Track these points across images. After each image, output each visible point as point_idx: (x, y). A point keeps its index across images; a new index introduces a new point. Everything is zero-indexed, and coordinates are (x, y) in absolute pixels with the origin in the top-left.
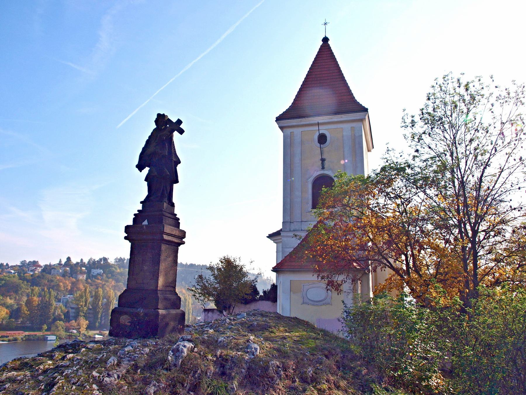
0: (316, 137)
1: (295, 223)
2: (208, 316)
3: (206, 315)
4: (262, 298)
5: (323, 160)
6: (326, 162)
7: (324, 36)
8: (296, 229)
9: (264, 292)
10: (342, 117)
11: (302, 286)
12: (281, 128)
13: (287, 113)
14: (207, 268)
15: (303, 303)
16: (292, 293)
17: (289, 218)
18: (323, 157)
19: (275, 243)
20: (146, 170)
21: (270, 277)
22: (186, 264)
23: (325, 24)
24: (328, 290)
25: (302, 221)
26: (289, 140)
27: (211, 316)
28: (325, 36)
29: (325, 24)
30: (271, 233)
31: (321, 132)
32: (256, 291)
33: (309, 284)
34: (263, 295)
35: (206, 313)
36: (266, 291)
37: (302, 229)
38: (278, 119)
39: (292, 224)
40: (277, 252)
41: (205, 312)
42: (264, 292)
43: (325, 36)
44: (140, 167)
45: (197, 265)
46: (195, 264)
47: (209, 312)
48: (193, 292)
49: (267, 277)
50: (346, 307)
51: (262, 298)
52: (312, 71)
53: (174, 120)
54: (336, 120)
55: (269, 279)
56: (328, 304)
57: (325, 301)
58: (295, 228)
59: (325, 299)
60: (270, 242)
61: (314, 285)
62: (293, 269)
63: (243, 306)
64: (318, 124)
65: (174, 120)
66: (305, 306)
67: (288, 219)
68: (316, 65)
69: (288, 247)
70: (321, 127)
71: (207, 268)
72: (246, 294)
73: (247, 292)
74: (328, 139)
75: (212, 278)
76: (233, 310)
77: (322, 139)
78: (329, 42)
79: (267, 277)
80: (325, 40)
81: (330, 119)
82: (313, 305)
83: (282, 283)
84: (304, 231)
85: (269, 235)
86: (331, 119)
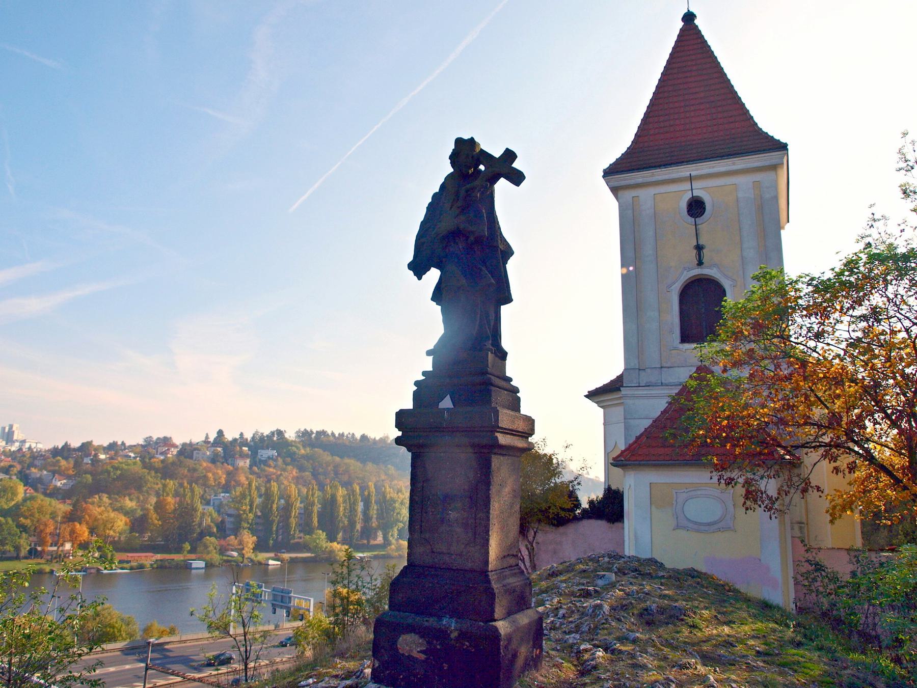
0: (684, 205)
5: (699, 248)
6: (705, 252)
7: (686, 11)
9: (591, 502)
10: (734, 164)
12: (615, 190)
15: (678, 527)
16: (653, 507)
18: (700, 243)
20: (433, 275)
24: (747, 509)
25: (662, 367)
28: (689, 11)
30: (592, 388)
31: (696, 193)
32: (577, 504)
33: (688, 490)
34: (587, 506)
36: (595, 500)
37: (663, 382)
38: (608, 173)
39: (642, 374)
42: (591, 502)
43: (689, 11)
44: (418, 268)
53: (497, 153)
56: (728, 529)
60: (592, 406)
61: (699, 492)
64: (691, 179)
65: (497, 153)
66: (682, 533)
70: (696, 184)
72: (563, 509)
77: (696, 207)
78: (696, 22)
80: (689, 18)
81: (710, 168)
82: (698, 531)
83: (633, 487)
85: (589, 392)
86: (713, 167)
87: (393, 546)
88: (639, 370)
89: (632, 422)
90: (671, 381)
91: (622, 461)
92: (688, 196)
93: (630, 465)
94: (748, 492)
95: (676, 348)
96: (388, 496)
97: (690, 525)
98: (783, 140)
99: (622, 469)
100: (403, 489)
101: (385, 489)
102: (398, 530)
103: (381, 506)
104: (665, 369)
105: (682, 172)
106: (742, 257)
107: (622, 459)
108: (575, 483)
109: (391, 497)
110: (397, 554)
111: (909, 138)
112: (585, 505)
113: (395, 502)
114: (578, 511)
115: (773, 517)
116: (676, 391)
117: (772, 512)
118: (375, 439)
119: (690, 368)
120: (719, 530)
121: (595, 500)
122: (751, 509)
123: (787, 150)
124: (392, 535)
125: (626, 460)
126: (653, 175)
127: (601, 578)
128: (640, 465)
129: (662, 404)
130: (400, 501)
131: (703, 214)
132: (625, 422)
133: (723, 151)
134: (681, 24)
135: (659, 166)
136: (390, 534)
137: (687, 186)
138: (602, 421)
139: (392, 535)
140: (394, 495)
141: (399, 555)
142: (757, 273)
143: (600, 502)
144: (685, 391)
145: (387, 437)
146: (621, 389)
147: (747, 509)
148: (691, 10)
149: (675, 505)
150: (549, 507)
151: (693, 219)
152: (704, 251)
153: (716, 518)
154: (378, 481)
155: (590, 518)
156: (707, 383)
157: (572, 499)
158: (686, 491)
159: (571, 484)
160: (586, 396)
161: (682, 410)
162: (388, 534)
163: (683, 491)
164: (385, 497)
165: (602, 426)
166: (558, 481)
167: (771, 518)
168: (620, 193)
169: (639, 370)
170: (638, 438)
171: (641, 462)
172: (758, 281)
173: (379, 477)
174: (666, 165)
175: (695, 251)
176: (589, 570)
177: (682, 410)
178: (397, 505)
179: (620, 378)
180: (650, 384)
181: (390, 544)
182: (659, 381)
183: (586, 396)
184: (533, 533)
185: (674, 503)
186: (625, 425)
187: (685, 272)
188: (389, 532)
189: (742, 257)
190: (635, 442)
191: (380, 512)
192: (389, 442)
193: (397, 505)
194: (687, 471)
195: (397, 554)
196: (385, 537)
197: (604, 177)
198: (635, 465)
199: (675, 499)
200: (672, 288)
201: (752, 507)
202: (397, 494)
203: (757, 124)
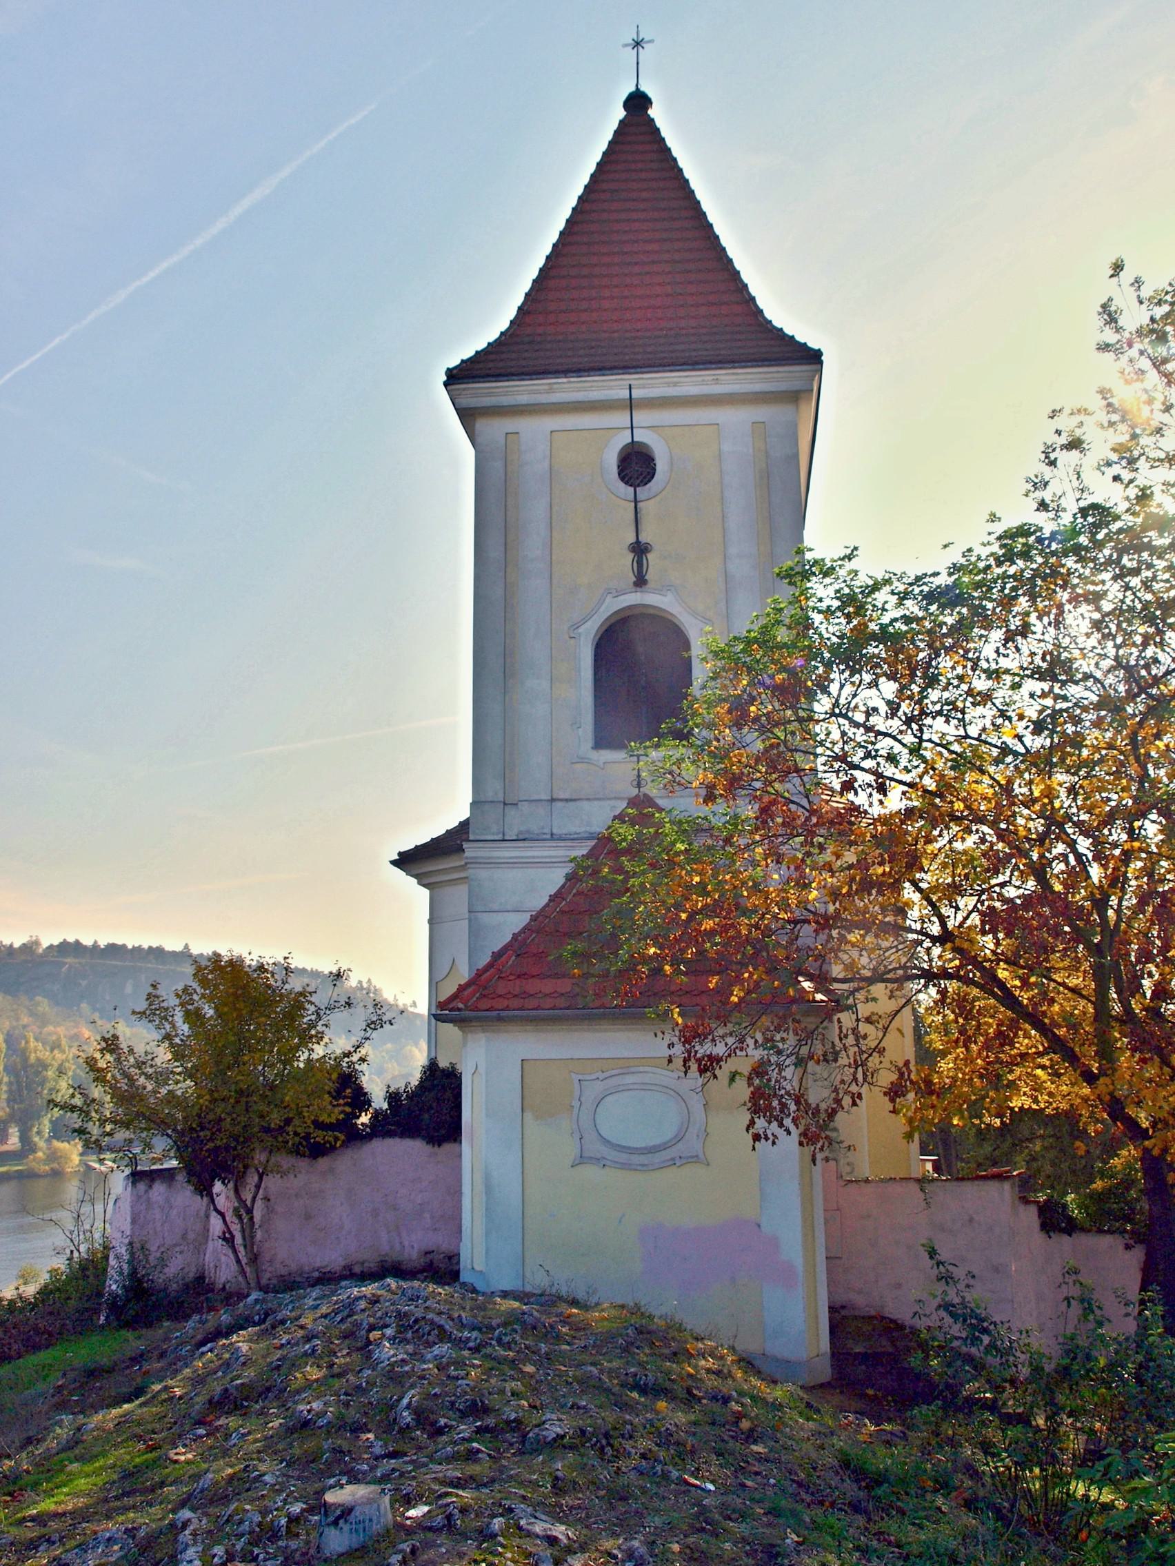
1: (524, 807)
2: (148, 1200)
3: (139, 1197)
4: (385, 1126)
5: (640, 550)
7: (633, 89)
8: (528, 832)
9: (393, 1097)
11: (577, 1086)
12: (467, 416)
13: (492, 357)
14: (134, 1013)
15: (582, 1159)
16: (529, 1116)
17: (498, 785)
18: (643, 538)
19: (424, 886)
21: (369, 981)
22: (95, 946)
23: (638, 44)
24: (757, 1138)
25: (553, 800)
26: (498, 465)
27: (161, 1199)
28: (637, 89)
29: (638, 44)
30: (408, 845)
32: (361, 1100)
33: (606, 1074)
34: (385, 1106)
35: (142, 1186)
36: (401, 1090)
37: (555, 831)
38: (454, 378)
39: (511, 812)
40: (431, 921)
41: (134, 1183)
42: (393, 1097)
43: (637, 89)
45: (130, 947)
46: (124, 946)
47: (153, 1180)
48: (75, 1115)
49: (360, 982)
50: (947, 1278)
51: (385, 1126)
52: (587, 206)
54: (694, 390)
55: (365, 985)
56: (695, 1159)
57: (674, 1149)
58: (522, 828)
59: (679, 1138)
60: (406, 883)
61: (630, 1079)
62: (535, 1013)
63: (303, 1164)
64: (631, 405)
66: (590, 1172)
67: (494, 789)
68: (604, 186)
69: (496, 907)
70: (641, 417)
71: (134, 1013)
72: (318, 1125)
73: (324, 1118)
74: (661, 465)
75: (163, 1055)
76: (258, 1187)
79: (360, 982)
80: (638, 103)
81: (668, 384)
82: (626, 1166)
83: (482, 1069)
84: (561, 839)
85: (400, 854)
86: (675, 384)
87: (40, 1154)
88: (505, 804)
89: (486, 919)
90: (573, 829)
91: (459, 1010)
92: (625, 438)
93: (478, 1019)
94: (756, 1095)
95: (583, 760)
96: (33, 1056)
97: (612, 1155)
98: (813, 345)
99: (460, 1028)
100: (64, 1042)
101: (27, 1042)
102: (51, 1121)
103: (17, 1076)
104: (560, 804)
105: (611, 388)
106: (727, 576)
107: (461, 1005)
108: (355, 1058)
109: (38, 1059)
110: (47, 1168)
111: (1127, 276)
112: (379, 1101)
113: (45, 1066)
114: (364, 1119)
115: (819, 1156)
116: (582, 850)
117: (819, 1146)
118: (11, 946)
119: (612, 803)
120: (673, 1162)
121: (401, 1090)
122: (767, 1139)
123: (821, 363)
124: (38, 1133)
125: (467, 1008)
126: (550, 390)
127: (335, 1523)
128: (500, 1019)
129: (555, 879)
130: (56, 1064)
131: (649, 481)
132: (470, 921)
133: (694, 354)
134: (621, 113)
135: (566, 372)
136: (35, 1130)
137: (622, 419)
138: (427, 916)
139: (38, 1133)
140: (45, 1055)
141: (52, 1169)
142: (790, 563)
143: (413, 1096)
144: (604, 845)
145: (37, 943)
146: (465, 845)
147: (757, 1138)
148: (642, 88)
149: (575, 1111)
150: (288, 1121)
151: (632, 489)
152: (650, 556)
153: (668, 1133)
154: (14, 1028)
155: (390, 1134)
156: (656, 832)
157: (341, 1101)
158: (602, 1076)
159: (346, 1059)
160: (395, 863)
161: (601, 894)
162: (30, 1129)
163: (594, 1077)
164: (25, 1059)
165: (427, 926)
166: (319, 1051)
167: (814, 1161)
168: (481, 424)
169: (505, 804)
170: (497, 956)
171: (503, 1014)
172: (790, 583)
173: (18, 1019)
174: (579, 371)
175: (631, 556)
176: (320, 1422)
177: (601, 894)
178: (50, 1073)
179: (464, 825)
180: (527, 836)
181: (33, 1149)
182: (547, 830)
183: (395, 863)
184: (256, 1178)
185: (576, 1104)
186: (470, 926)
187: (609, 599)
188: (33, 1126)
189: (727, 576)
190: (490, 965)
191: (14, 1087)
192: (40, 951)
193: (50, 1073)
194: (606, 1031)
195: (47, 1168)
196: (25, 1138)
197: (446, 384)
198: (486, 1019)
199: (577, 1093)
200: (580, 630)
201: (769, 1133)
202: (52, 1050)
203: (762, 311)
